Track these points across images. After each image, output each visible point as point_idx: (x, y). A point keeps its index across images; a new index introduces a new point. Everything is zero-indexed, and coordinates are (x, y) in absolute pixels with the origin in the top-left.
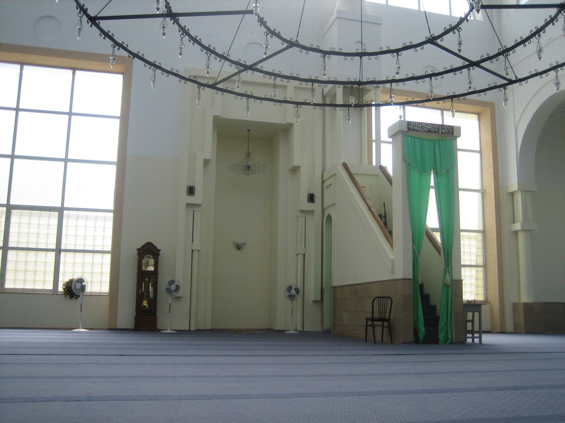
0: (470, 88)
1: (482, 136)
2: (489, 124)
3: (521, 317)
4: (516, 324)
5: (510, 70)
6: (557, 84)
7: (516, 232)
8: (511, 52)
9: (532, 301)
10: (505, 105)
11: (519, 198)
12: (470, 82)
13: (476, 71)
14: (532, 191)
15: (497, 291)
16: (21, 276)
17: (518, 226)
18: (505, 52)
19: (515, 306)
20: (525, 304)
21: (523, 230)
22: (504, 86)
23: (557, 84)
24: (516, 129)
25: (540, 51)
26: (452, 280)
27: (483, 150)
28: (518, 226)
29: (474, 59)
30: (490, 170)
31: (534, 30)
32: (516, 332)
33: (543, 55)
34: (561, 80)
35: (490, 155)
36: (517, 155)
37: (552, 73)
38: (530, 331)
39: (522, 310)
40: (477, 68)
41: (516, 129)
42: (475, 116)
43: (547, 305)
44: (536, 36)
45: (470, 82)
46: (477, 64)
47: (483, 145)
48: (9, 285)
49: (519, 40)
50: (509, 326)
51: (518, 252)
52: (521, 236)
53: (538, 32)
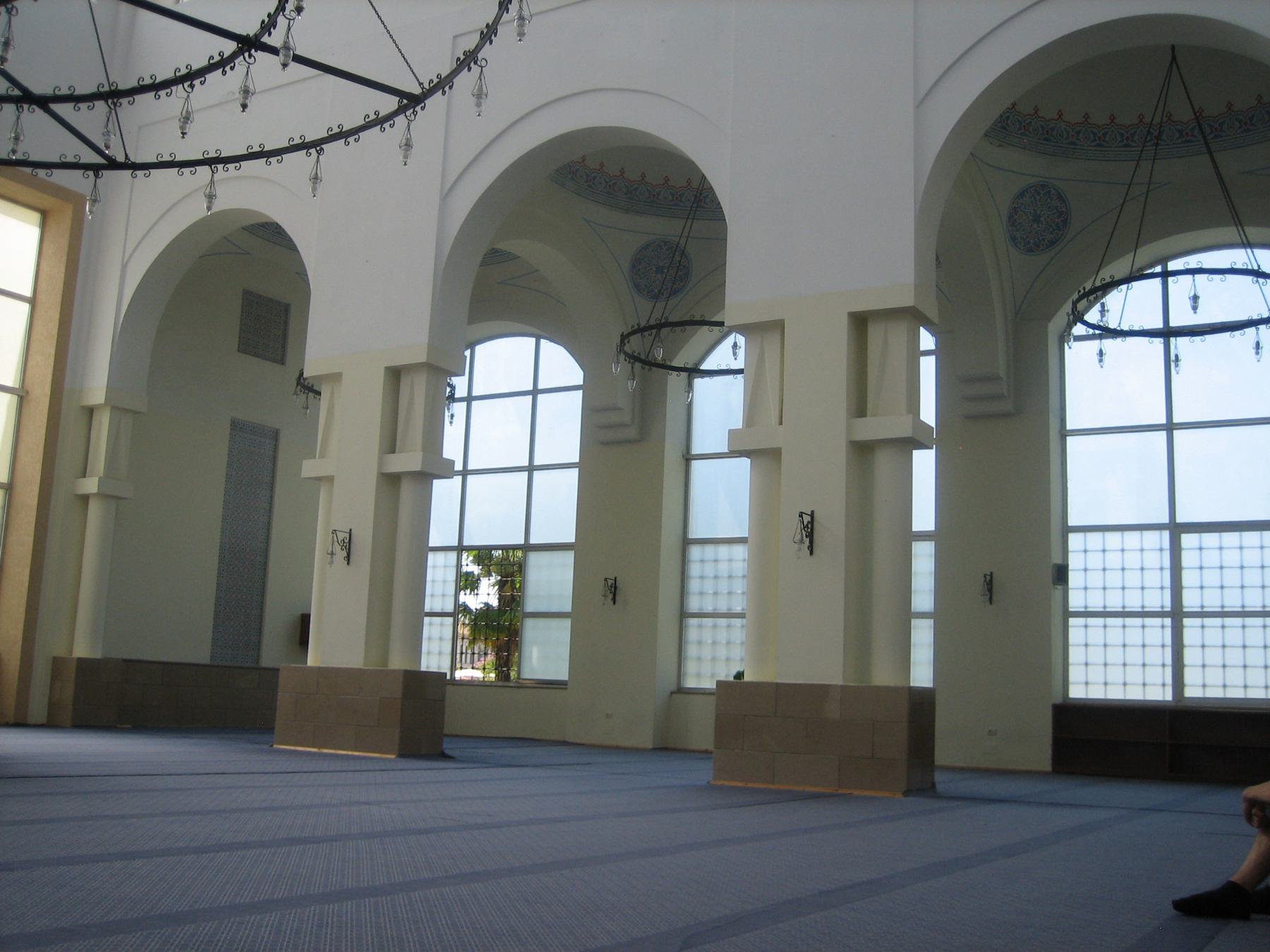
0: (14, 152)
1: (44, 266)
2: (64, 242)
3: (68, 692)
4: (53, 707)
5: (115, 140)
6: (211, 197)
7: (85, 499)
8: (124, 101)
9: (98, 655)
10: (91, 212)
11: (103, 423)
12: (17, 139)
13: (34, 118)
14: (135, 413)
15: (21, 626)
16: (1095, 579)
17: (90, 485)
18: (113, 96)
19: (57, 664)
20: (80, 660)
21: (101, 495)
22: (96, 169)
23: (211, 197)
24: (124, 267)
25: (186, 119)
26: (519, 678)
27: (41, 298)
28: (90, 485)
29: (38, 89)
30: (46, 348)
31: (184, 71)
32: (51, 724)
33: (190, 129)
34: (219, 190)
35: (55, 315)
36: (115, 324)
37: (204, 171)
38: (84, 722)
39: (71, 673)
40: (39, 112)
41: (124, 267)
42: (36, 217)
43: (130, 666)
44: (186, 85)
45: (17, 139)
46: (43, 102)
47: (42, 285)
48: (914, 529)
49: (148, 81)
50: (38, 709)
51: (84, 539)
52: (95, 509)
53: (191, 77)
